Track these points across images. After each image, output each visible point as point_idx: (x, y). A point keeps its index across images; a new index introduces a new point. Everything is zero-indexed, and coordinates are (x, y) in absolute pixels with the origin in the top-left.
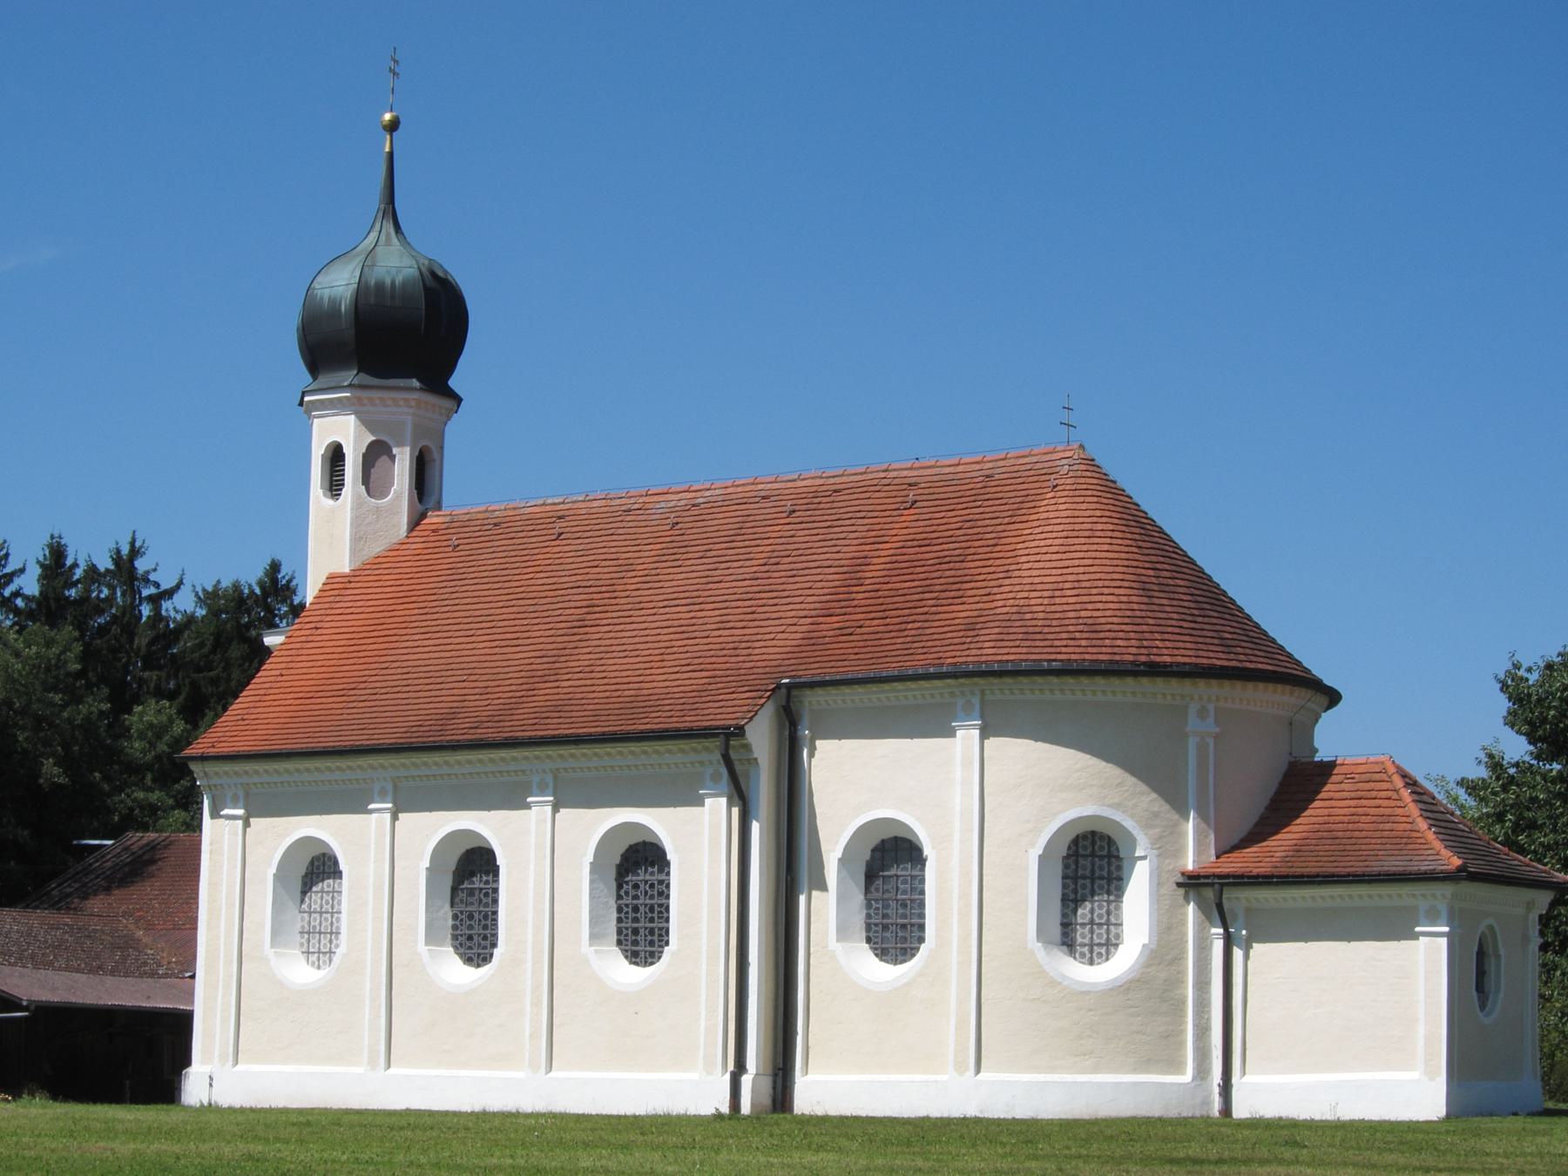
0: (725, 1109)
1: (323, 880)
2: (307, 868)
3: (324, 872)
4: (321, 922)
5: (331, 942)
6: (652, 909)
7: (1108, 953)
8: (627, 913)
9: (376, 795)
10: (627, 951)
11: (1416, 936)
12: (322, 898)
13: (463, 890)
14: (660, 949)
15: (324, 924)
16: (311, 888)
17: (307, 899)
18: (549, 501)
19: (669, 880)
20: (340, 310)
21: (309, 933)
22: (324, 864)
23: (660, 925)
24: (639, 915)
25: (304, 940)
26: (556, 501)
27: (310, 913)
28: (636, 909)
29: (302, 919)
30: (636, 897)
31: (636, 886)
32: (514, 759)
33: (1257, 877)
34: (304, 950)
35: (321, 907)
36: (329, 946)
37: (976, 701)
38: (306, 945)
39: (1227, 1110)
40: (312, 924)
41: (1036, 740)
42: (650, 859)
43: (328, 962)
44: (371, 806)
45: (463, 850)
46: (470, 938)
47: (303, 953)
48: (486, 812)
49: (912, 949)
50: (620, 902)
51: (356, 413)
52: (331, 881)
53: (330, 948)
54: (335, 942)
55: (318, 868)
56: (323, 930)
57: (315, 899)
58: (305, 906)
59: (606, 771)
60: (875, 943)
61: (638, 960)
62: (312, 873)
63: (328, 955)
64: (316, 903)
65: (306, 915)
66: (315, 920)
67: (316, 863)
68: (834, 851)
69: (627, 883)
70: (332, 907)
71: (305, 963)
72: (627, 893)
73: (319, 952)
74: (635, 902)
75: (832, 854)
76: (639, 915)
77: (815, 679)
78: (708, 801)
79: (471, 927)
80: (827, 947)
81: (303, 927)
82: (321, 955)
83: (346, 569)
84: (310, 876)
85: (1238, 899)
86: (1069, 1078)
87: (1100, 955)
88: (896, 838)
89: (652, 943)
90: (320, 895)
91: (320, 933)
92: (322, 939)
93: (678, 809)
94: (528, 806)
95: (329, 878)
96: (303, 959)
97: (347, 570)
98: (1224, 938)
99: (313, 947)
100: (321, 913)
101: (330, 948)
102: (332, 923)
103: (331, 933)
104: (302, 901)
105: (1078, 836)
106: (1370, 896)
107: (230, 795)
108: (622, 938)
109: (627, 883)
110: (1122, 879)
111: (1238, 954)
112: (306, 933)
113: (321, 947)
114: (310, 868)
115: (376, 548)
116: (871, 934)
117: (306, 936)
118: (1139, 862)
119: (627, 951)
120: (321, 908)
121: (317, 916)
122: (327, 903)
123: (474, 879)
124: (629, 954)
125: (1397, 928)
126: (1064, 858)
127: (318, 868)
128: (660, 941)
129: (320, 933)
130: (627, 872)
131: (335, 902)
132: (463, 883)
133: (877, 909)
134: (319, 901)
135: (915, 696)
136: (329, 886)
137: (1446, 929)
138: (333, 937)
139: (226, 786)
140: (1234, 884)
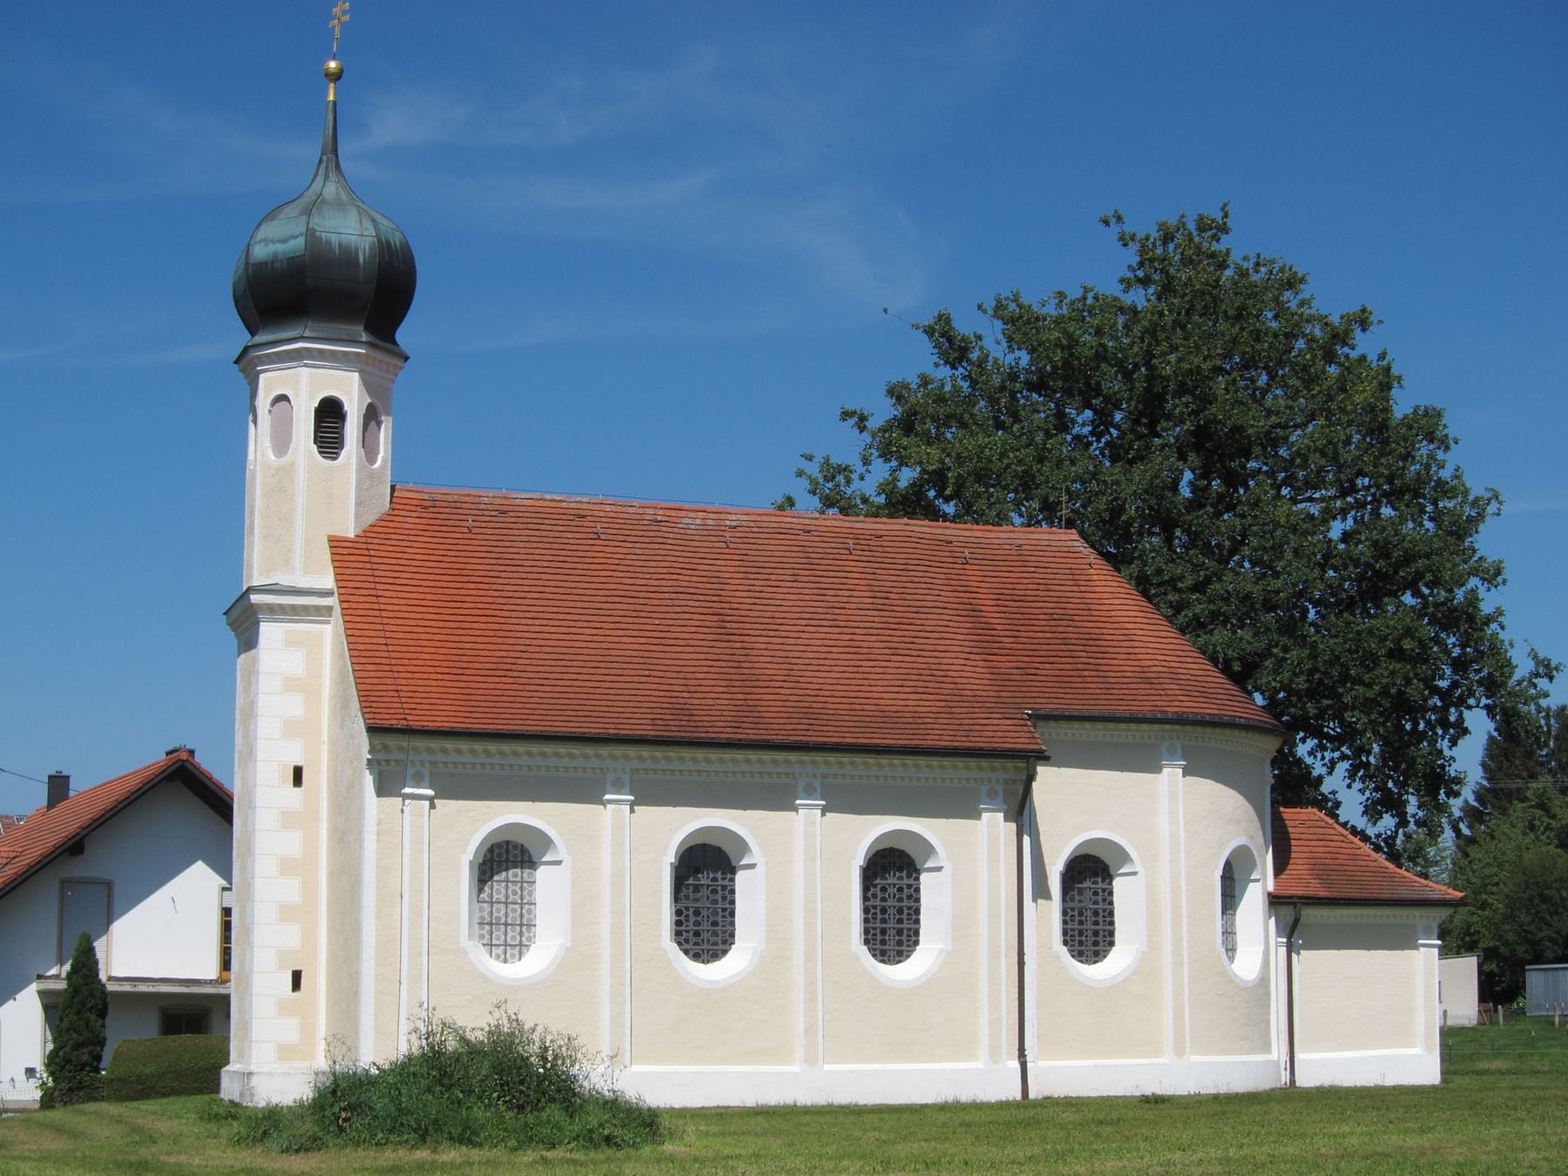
0: (1019, 1097)
1: (507, 869)
2: (485, 855)
3: (507, 861)
4: (506, 913)
5: (521, 934)
6: (900, 911)
7: (521, 954)
8: (875, 914)
9: (409, 777)
10: (875, 950)
11: (1416, 947)
12: (507, 888)
13: (688, 885)
14: (908, 949)
15: (511, 915)
16: (492, 877)
17: (486, 888)
18: (548, 497)
19: (734, 886)
20: (357, 259)
21: (491, 924)
22: (507, 853)
23: (909, 926)
24: (887, 916)
25: (484, 932)
26: (584, 500)
27: (492, 903)
28: (884, 911)
29: (481, 909)
30: (900, 900)
31: (884, 889)
32: (787, 762)
33: (1323, 899)
34: (485, 942)
35: (507, 898)
36: (518, 938)
37: (1178, 745)
38: (488, 937)
39: (1293, 1081)
40: (495, 915)
41: (1217, 781)
42: (897, 865)
43: (517, 956)
44: (607, 797)
45: (901, 847)
46: (900, 932)
47: (484, 945)
48: (742, 811)
49: (1104, 951)
50: (867, 903)
51: (361, 372)
52: (518, 871)
53: (521, 940)
54: (526, 934)
55: (500, 855)
56: (510, 922)
57: (498, 886)
58: (484, 896)
59: (594, 773)
60: (1072, 946)
61: (886, 958)
62: (492, 861)
63: (518, 948)
64: (499, 892)
65: (485, 905)
66: (499, 911)
67: (496, 851)
68: (1055, 865)
69: (875, 886)
70: (522, 897)
71: (488, 956)
72: (875, 896)
73: (506, 945)
74: (884, 904)
75: (1053, 868)
76: (887, 916)
77: (1055, 713)
78: (985, 816)
79: (884, 921)
80: (1051, 949)
81: (482, 917)
82: (508, 948)
83: (351, 534)
84: (489, 864)
85: (1310, 914)
86: (1222, 1058)
87: (513, 956)
88: (704, 845)
89: (900, 943)
90: (503, 884)
91: (506, 925)
92: (509, 931)
93: (951, 820)
94: (795, 809)
95: (516, 868)
96: (484, 951)
97: (351, 535)
98: (1287, 947)
99: (498, 939)
100: (506, 903)
101: (521, 940)
102: (522, 916)
103: (521, 925)
104: (481, 890)
105: (492, 846)
106: (1388, 916)
107: (410, 771)
108: (870, 937)
109: (875, 886)
110: (1234, 897)
111: (1294, 956)
112: (487, 924)
113: (509, 940)
114: (489, 856)
115: (371, 518)
116: (1068, 938)
117: (487, 927)
118: (1251, 884)
119: (875, 950)
120: (507, 898)
121: (502, 907)
122: (515, 893)
123: (700, 876)
124: (878, 952)
125: (1403, 940)
126: (480, 864)
127: (500, 855)
128: (908, 941)
129: (506, 925)
130: (875, 876)
131: (525, 893)
132: (688, 879)
133: (1073, 916)
134: (503, 891)
135: (1142, 737)
136: (515, 875)
137: (1439, 942)
138: (524, 929)
139: (797, 775)
140: (1309, 904)
